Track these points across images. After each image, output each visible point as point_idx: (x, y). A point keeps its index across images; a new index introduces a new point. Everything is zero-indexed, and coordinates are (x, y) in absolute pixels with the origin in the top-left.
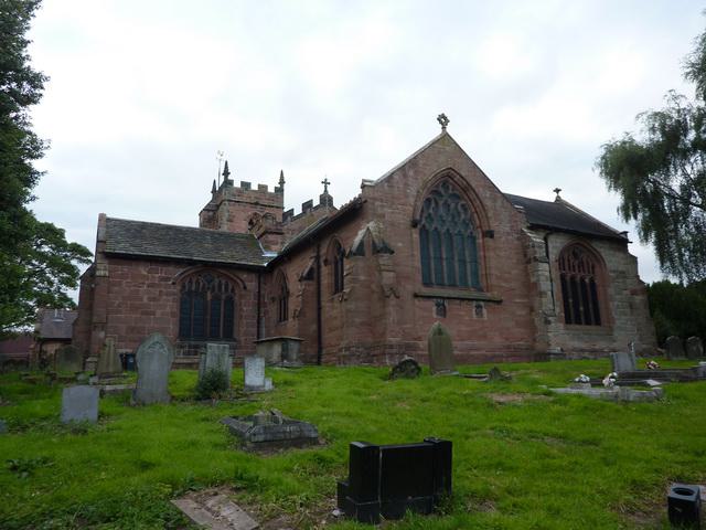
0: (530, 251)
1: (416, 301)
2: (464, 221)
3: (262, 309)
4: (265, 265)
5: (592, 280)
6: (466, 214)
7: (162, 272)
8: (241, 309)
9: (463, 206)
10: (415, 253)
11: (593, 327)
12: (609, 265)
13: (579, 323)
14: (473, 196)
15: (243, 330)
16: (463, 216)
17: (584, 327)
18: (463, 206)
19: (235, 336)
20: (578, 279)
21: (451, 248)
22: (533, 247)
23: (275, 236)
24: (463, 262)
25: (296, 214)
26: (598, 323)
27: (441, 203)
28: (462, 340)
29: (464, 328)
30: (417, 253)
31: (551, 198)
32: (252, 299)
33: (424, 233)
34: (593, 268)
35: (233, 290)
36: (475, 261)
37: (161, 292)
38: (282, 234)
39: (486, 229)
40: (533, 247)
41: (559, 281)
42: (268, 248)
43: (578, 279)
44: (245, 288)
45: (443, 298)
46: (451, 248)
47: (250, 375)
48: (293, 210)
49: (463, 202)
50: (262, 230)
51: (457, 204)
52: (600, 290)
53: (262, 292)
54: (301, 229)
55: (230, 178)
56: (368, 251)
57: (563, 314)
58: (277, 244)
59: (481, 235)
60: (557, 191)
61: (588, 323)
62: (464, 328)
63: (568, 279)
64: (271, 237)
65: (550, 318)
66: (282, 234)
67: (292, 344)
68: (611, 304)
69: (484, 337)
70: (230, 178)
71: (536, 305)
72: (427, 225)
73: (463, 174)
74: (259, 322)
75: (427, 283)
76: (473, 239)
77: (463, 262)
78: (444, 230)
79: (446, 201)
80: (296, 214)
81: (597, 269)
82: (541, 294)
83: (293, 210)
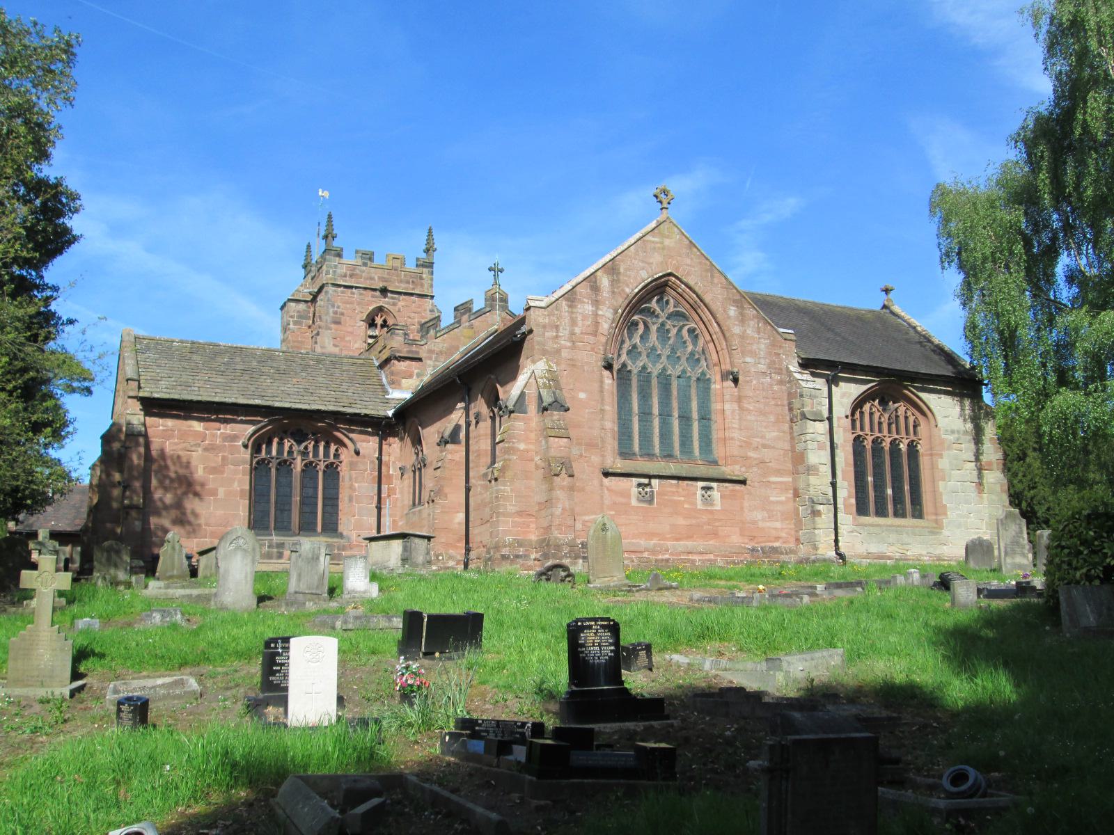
0: (796, 403)
1: (606, 481)
2: (692, 354)
3: (385, 487)
4: (390, 413)
5: (912, 447)
6: (695, 343)
7: (221, 431)
8: (351, 487)
9: (691, 331)
10: (607, 408)
11: (909, 521)
12: (942, 422)
13: (881, 512)
14: (706, 315)
15: (671, 783)
16: (690, 348)
17: (891, 520)
18: (691, 331)
19: (341, 528)
20: (886, 445)
21: (645, 396)
22: (801, 396)
23: (408, 362)
24: (685, 418)
25: (475, 308)
26: (918, 514)
27: (654, 328)
28: (678, 539)
29: (681, 521)
30: (611, 408)
31: (870, 302)
32: (370, 471)
33: (623, 376)
34: (915, 427)
35: (337, 456)
36: (705, 418)
37: (224, 458)
38: (420, 360)
39: (726, 366)
40: (801, 396)
41: (850, 449)
42: (395, 383)
43: (886, 445)
44: (357, 453)
45: (650, 477)
46: (645, 396)
47: (351, 579)
48: (471, 302)
49: (693, 325)
50: (384, 356)
51: (680, 330)
52: (924, 462)
53: (385, 458)
54: (450, 351)
55: (336, 244)
56: (532, 407)
57: (853, 501)
58: (410, 377)
59: (718, 377)
60: (887, 291)
61: (899, 513)
62: (681, 521)
63: (868, 444)
64: (403, 365)
65: (820, 508)
66: (420, 360)
67: (417, 540)
68: (941, 484)
69: (715, 534)
70: (336, 244)
71: (801, 485)
72: (629, 362)
73: (691, 283)
74: (379, 509)
75: (625, 453)
76: (704, 381)
77: (685, 418)
78: (655, 370)
79: (663, 324)
80: (475, 308)
81: (922, 429)
82: (811, 470)
83: (471, 302)
